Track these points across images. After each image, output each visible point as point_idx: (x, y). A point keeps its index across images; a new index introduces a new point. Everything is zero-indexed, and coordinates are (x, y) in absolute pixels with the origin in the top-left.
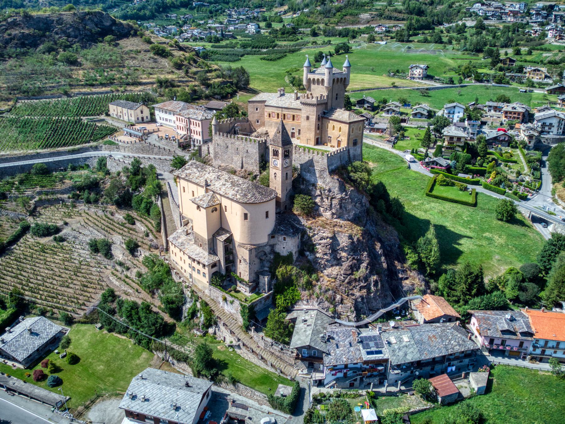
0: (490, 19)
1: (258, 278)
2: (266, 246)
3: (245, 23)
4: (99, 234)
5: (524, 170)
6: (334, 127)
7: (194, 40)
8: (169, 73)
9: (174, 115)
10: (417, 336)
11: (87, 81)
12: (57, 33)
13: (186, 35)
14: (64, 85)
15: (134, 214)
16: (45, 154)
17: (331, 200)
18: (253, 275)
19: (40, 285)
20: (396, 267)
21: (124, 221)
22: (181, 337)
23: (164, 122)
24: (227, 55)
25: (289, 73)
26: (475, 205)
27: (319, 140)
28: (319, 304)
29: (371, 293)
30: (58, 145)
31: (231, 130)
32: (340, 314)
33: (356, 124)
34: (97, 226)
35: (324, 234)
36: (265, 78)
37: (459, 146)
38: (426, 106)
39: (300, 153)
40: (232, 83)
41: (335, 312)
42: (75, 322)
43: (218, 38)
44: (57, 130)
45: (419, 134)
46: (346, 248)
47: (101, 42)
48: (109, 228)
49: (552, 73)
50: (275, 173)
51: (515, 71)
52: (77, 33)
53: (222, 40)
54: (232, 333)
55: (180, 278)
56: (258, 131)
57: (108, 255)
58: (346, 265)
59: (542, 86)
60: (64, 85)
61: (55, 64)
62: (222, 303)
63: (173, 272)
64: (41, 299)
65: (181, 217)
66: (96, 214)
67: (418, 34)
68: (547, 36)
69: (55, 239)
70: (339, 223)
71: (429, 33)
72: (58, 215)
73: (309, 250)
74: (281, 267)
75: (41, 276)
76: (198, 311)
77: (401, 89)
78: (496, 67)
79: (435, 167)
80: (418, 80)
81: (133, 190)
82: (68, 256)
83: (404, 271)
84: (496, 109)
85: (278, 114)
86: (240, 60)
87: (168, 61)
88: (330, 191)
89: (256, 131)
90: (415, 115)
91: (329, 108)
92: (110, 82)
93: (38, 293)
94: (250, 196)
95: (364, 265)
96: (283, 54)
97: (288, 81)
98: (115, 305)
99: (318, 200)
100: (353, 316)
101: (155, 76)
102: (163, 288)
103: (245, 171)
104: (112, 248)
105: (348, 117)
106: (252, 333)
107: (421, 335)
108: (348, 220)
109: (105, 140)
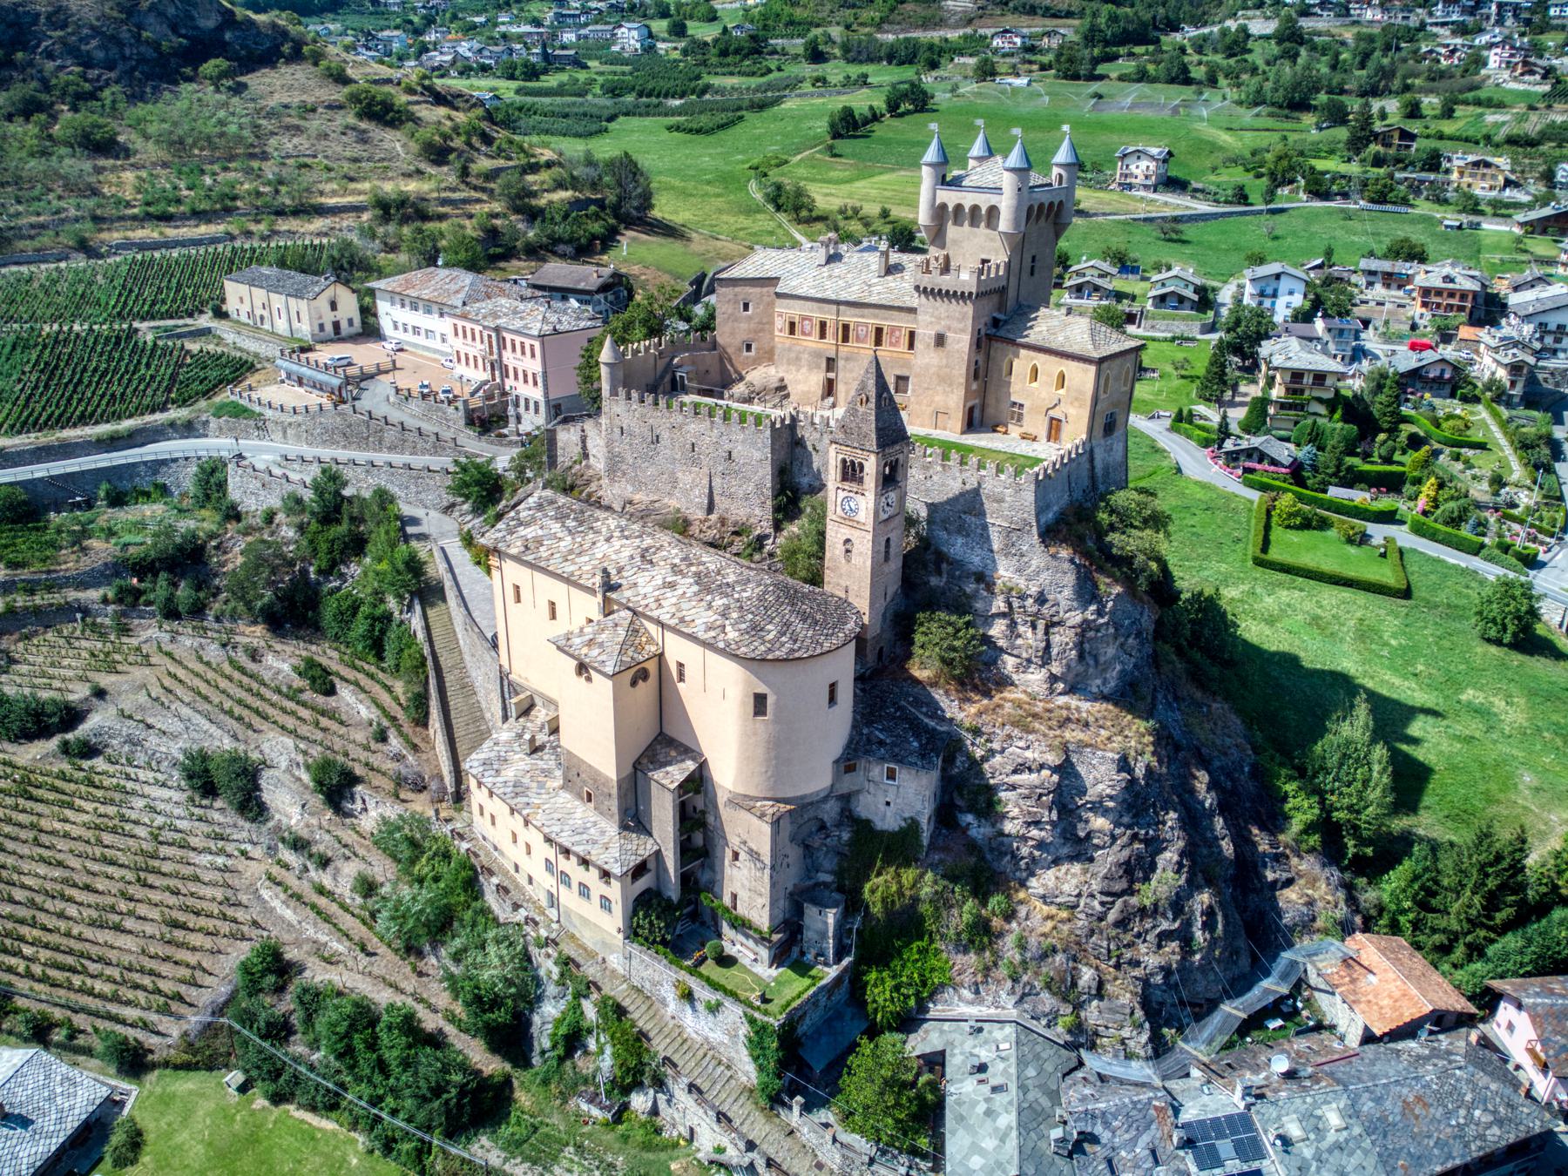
0: (1315, 14)
1: (798, 911)
2: (825, 799)
3: (607, 23)
4: (213, 729)
5: (1512, 472)
6: (1035, 371)
7: (461, 73)
8: (407, 176)
9: (441, 315)
10: (1367, 1106)
11: (148, 204)
12: (50, 55)
13: (438, 58)
14: (77, 220)
15: (328, 655)
16: (19, 454)
17: (1047, 633)
18: (782, 903)
19: (22, 922)
20: (1254, 845)
21: (299, 683)
22: (535, 1129)
23: (409, 337)
24: (566, 116)
25: (760, 172)
26: (1406, 594)
27: (977, 414)
28: (1020, 1001)
29: (1194, 953)
30: (62, 422)
31: (662, 377)
32: (1096, 1034)
33: (1118, 361)
34: (206, 698)
35: (1029, 754)
36: (690, 185)
37: (1320, 400)
38: (1183, 272)
39: (926, 467)
40: (601, 204)
41: (1078, 1028)
42: (153, 1066)
43: (534, 65)
44: (56, 367)
45: (1186, 360)
46: (1111, 804)
47: (190, 80)
48: (248, 707)
49: (1523, 172)
50: (848, 541)
51: (1419, 165)
52: (114, 51)
53: (545, 72)
54: (722, 1117)
55: (516, 907)
56: (748, 378)
57: (252, 806)
58: (1108, 859)
59: (1503, 211)
60: (77, 220)
61: (45, 153)
62: (673, 1005)
63: (489, 885)
64: (29, 975)
65: (508, 688)
66: (200, 659)
67: (1115, 57)
68: (1485, 64)
69: (65, 749)
70: (1078, 709)
71: (1147, 53)
72: (72, 664)
73: (971, 809)
74: (879, 874)
75: (23, 886)
76: (590, 1031)
77: (1100, 219)
78: (1362, 155)
79: (1258, 466)
80: (1142, 193)
81: (320, 572)
82: (111, 810)
83: (1278, 858)
84: (1389, 279)
85: (823, 325)
86: (606, 130)
87: (404, 139)
88: (1041, 599)
89: (742, 378)
90: (1161, 300)
91: (1010, 303)
92: (224, 207)
93: (17, 953)
94: (772, 631)
95: (1169, 856)
96: (731, 115)
97: (759, 197)
98: (287, 1004)
99: (997, 630)
100: (1140, 1041)
101: (366, 186)
102: (458, 943)
103: (723, 521)
104: (263, 783)
105: (1087, 337)
106: (794, 1117)
107: (1378, 1100)
108: (1105, 698)
109: (217, 399)
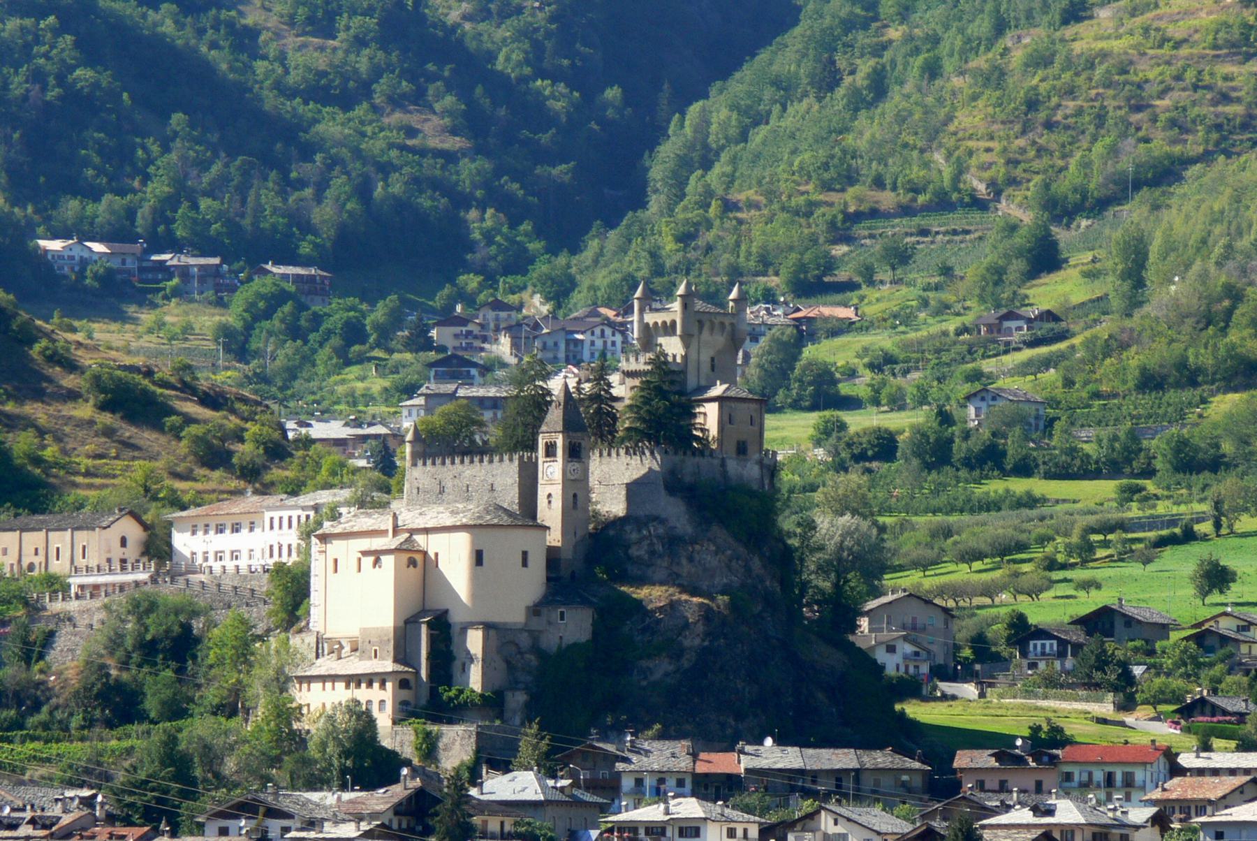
2: (521, 630)
